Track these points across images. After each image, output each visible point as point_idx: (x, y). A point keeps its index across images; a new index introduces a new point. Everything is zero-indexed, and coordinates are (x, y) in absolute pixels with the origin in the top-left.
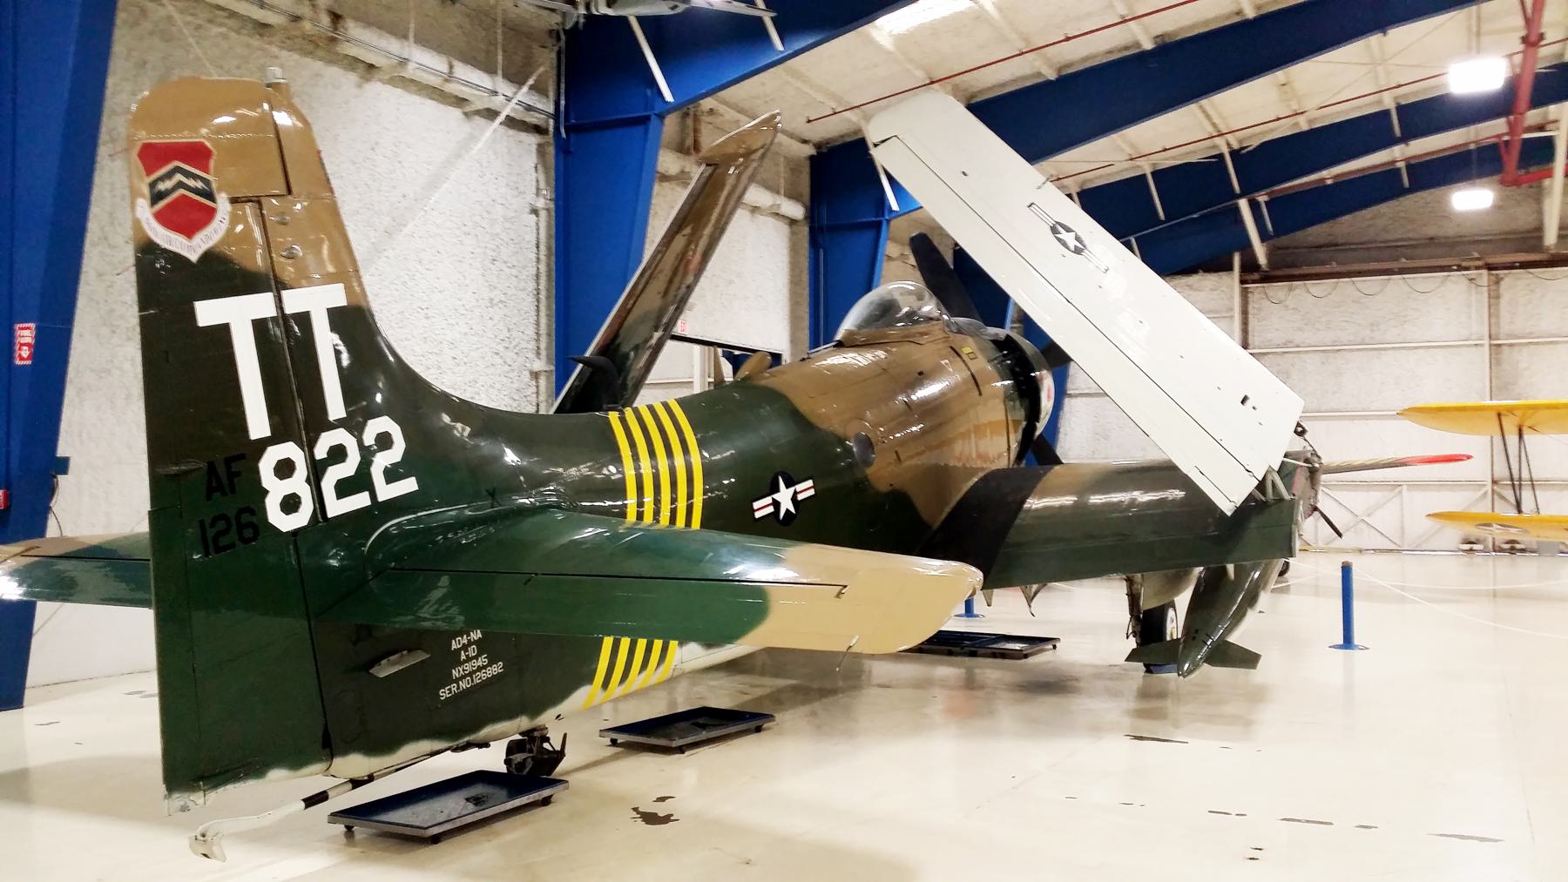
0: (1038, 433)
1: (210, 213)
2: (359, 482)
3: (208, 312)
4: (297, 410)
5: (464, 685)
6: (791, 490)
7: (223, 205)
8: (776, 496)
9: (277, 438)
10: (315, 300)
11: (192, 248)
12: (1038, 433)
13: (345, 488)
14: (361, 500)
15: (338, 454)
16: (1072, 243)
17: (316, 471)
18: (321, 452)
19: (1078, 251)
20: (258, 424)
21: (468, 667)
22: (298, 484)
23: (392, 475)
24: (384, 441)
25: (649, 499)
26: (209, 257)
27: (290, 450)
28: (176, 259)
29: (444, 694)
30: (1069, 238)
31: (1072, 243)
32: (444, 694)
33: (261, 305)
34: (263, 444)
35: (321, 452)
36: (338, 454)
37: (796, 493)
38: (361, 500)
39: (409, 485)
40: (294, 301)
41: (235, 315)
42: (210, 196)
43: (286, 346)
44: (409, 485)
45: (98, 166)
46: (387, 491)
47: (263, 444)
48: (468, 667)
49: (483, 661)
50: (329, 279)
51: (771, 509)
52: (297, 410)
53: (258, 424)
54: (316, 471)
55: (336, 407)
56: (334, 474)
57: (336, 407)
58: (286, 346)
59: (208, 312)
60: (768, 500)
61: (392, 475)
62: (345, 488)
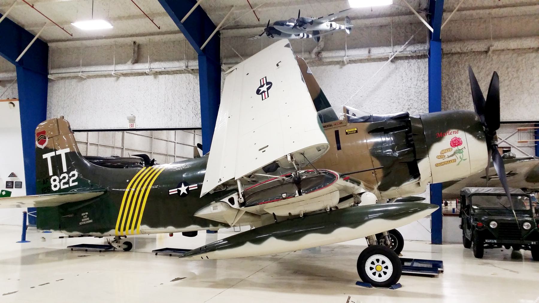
0: (485, 97)
1: (45, 141)
2: (67, 183)
3: (44, 156)
4: (58, 170)
5: (84, 223)
6: (187, 187)
7: (47, 139)
8: (179, 189)
9: (53, 175)
10: (62, 152)
11: (42, 147)
12: (485, 97)
13: (64, 184)
14: (67, 186)
15: (64, 178)
16: (262, 89)
17: (60, 180)
18: (70, 175)
19: (258, 92)
20: (51, 173)
21: (85, 219)
22: (57, 183)
23: (73, 181)
24: (74, 175)
25: (133, 189)
26: (45, 148)
27: (56, 177)
28: (41, 149)
29: (80, 224)
30: (265, 88)
31: (262, 89)
32: (80, 224)
33: (53, 154)
34: (51, 176)
35: (61, 177)
36: (64, 178)
37: (188, 188)
38: (67, 186)
39: (76, 183)
40: (58, 153)
41: (48, 156)
42: (45, 138)
43: (57, 160)
44: (76, 183)
45: (457, 113)
46: (71, 184)
47: (51, 176)
48: (85, 219)
49: (88, 219)
50: (68, 147)
51: (177, 192)
52: (58, 170)
53: (51, 173)
54: (60, 180)
55: (65, 169)
56: (63, 181)
57: (65, 169)
58: (57, 160)
59: (44, 156)
60: (176, 189)
61: (73, 181)
62: (64, 184)
